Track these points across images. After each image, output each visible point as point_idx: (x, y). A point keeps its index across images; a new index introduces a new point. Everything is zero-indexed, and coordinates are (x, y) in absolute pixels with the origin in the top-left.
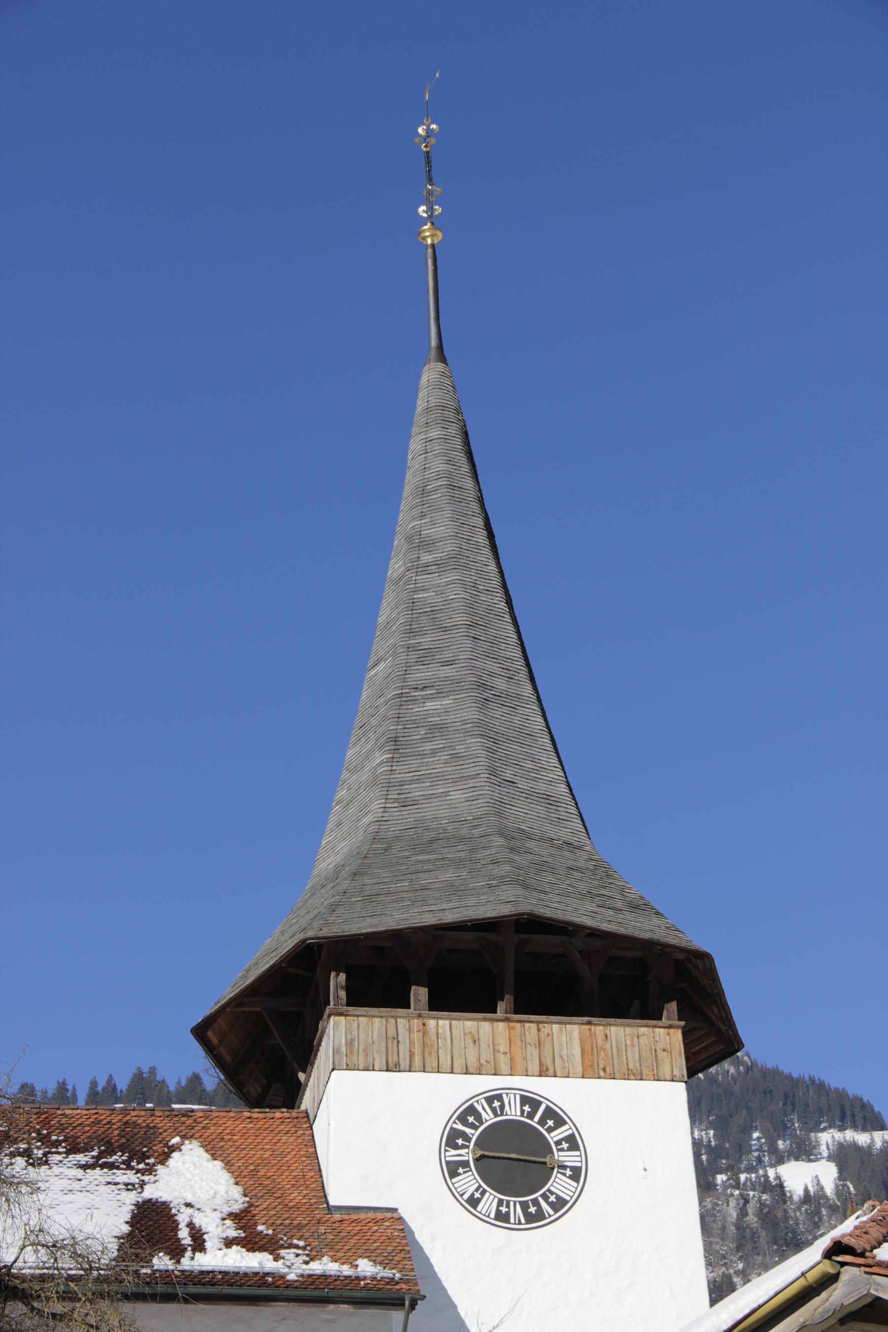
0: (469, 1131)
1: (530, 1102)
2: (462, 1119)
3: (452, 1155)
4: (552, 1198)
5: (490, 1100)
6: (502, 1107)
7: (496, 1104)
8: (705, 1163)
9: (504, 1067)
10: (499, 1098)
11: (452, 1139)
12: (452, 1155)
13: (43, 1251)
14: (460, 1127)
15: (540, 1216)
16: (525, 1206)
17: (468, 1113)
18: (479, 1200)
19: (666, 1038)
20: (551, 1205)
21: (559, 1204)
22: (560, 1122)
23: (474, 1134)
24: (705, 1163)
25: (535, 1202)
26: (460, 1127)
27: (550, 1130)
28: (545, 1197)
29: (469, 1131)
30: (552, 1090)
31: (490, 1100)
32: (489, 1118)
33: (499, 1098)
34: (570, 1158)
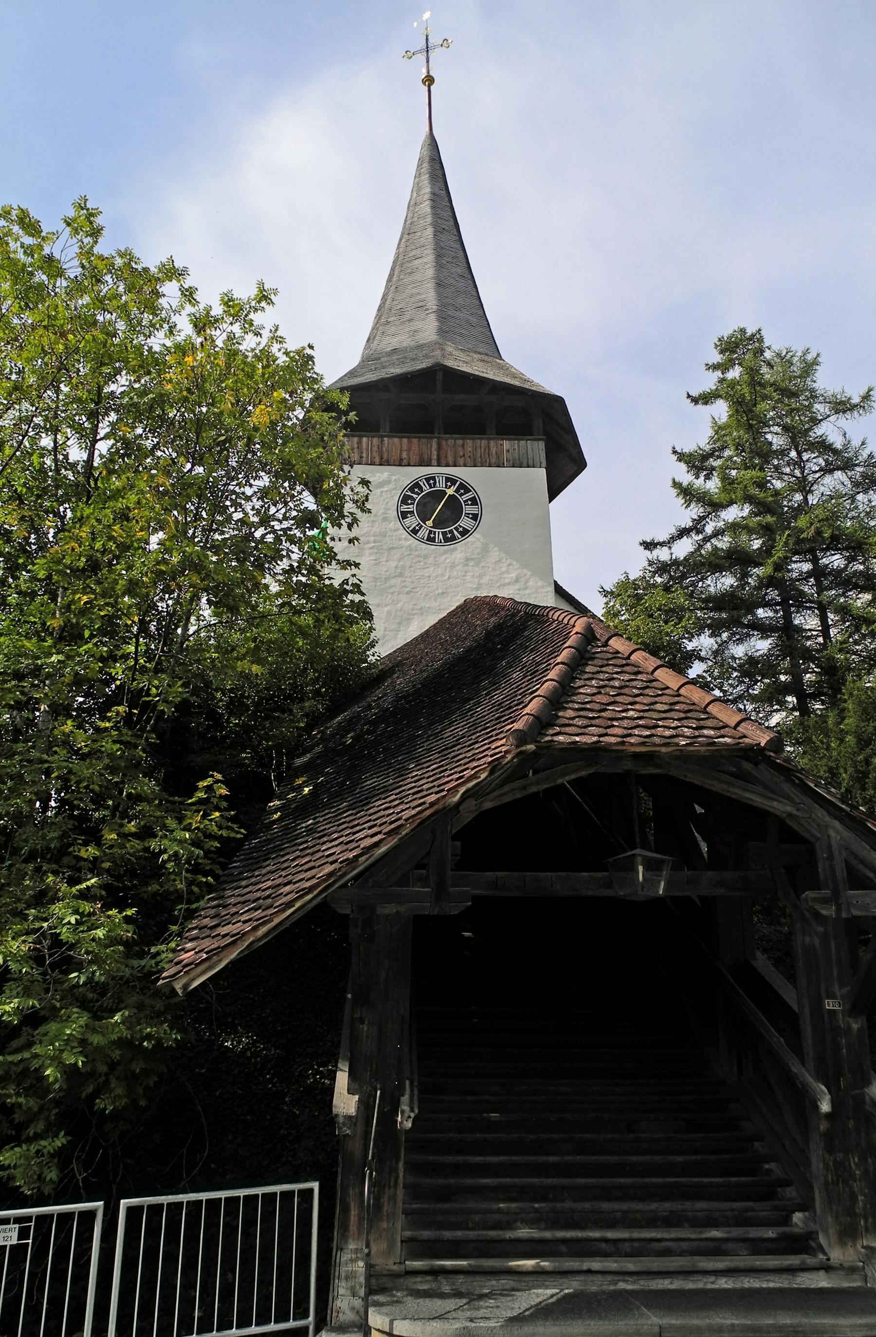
0: (415, 496)
1: (451, 481)
2: (411, 489)
3: (404, 508)
4: (461, 529)
5: (428, 480)
6: (435, 483)
7: (432, 482)
8: (706, 855)
9: (434, 462)
10: (434, 478)
11: (405, 500)
12: (404, 508)
13: (820, 418)
14: (409, 493)
15: (453, 538)
16: (444, 534)
17: (415, 486)
18: (418, 531)
19: (537, 448)
20: (460, 533)
21: (465, 532)
22: (467, 491)
23: (418, 498)
24: (706, 855)
25: (451, 532)
26: (409, 493)
27: (461, 495)
28: (456, 529)
29: (415, 496)
30: (461, 472)
31: (428, 480)
32: (427, 489)
33: (434, 478)
34: (423, 533)
